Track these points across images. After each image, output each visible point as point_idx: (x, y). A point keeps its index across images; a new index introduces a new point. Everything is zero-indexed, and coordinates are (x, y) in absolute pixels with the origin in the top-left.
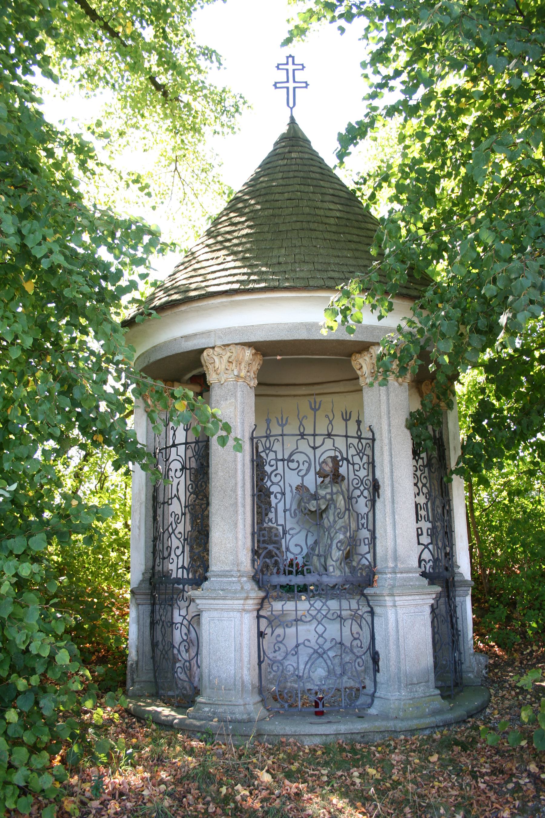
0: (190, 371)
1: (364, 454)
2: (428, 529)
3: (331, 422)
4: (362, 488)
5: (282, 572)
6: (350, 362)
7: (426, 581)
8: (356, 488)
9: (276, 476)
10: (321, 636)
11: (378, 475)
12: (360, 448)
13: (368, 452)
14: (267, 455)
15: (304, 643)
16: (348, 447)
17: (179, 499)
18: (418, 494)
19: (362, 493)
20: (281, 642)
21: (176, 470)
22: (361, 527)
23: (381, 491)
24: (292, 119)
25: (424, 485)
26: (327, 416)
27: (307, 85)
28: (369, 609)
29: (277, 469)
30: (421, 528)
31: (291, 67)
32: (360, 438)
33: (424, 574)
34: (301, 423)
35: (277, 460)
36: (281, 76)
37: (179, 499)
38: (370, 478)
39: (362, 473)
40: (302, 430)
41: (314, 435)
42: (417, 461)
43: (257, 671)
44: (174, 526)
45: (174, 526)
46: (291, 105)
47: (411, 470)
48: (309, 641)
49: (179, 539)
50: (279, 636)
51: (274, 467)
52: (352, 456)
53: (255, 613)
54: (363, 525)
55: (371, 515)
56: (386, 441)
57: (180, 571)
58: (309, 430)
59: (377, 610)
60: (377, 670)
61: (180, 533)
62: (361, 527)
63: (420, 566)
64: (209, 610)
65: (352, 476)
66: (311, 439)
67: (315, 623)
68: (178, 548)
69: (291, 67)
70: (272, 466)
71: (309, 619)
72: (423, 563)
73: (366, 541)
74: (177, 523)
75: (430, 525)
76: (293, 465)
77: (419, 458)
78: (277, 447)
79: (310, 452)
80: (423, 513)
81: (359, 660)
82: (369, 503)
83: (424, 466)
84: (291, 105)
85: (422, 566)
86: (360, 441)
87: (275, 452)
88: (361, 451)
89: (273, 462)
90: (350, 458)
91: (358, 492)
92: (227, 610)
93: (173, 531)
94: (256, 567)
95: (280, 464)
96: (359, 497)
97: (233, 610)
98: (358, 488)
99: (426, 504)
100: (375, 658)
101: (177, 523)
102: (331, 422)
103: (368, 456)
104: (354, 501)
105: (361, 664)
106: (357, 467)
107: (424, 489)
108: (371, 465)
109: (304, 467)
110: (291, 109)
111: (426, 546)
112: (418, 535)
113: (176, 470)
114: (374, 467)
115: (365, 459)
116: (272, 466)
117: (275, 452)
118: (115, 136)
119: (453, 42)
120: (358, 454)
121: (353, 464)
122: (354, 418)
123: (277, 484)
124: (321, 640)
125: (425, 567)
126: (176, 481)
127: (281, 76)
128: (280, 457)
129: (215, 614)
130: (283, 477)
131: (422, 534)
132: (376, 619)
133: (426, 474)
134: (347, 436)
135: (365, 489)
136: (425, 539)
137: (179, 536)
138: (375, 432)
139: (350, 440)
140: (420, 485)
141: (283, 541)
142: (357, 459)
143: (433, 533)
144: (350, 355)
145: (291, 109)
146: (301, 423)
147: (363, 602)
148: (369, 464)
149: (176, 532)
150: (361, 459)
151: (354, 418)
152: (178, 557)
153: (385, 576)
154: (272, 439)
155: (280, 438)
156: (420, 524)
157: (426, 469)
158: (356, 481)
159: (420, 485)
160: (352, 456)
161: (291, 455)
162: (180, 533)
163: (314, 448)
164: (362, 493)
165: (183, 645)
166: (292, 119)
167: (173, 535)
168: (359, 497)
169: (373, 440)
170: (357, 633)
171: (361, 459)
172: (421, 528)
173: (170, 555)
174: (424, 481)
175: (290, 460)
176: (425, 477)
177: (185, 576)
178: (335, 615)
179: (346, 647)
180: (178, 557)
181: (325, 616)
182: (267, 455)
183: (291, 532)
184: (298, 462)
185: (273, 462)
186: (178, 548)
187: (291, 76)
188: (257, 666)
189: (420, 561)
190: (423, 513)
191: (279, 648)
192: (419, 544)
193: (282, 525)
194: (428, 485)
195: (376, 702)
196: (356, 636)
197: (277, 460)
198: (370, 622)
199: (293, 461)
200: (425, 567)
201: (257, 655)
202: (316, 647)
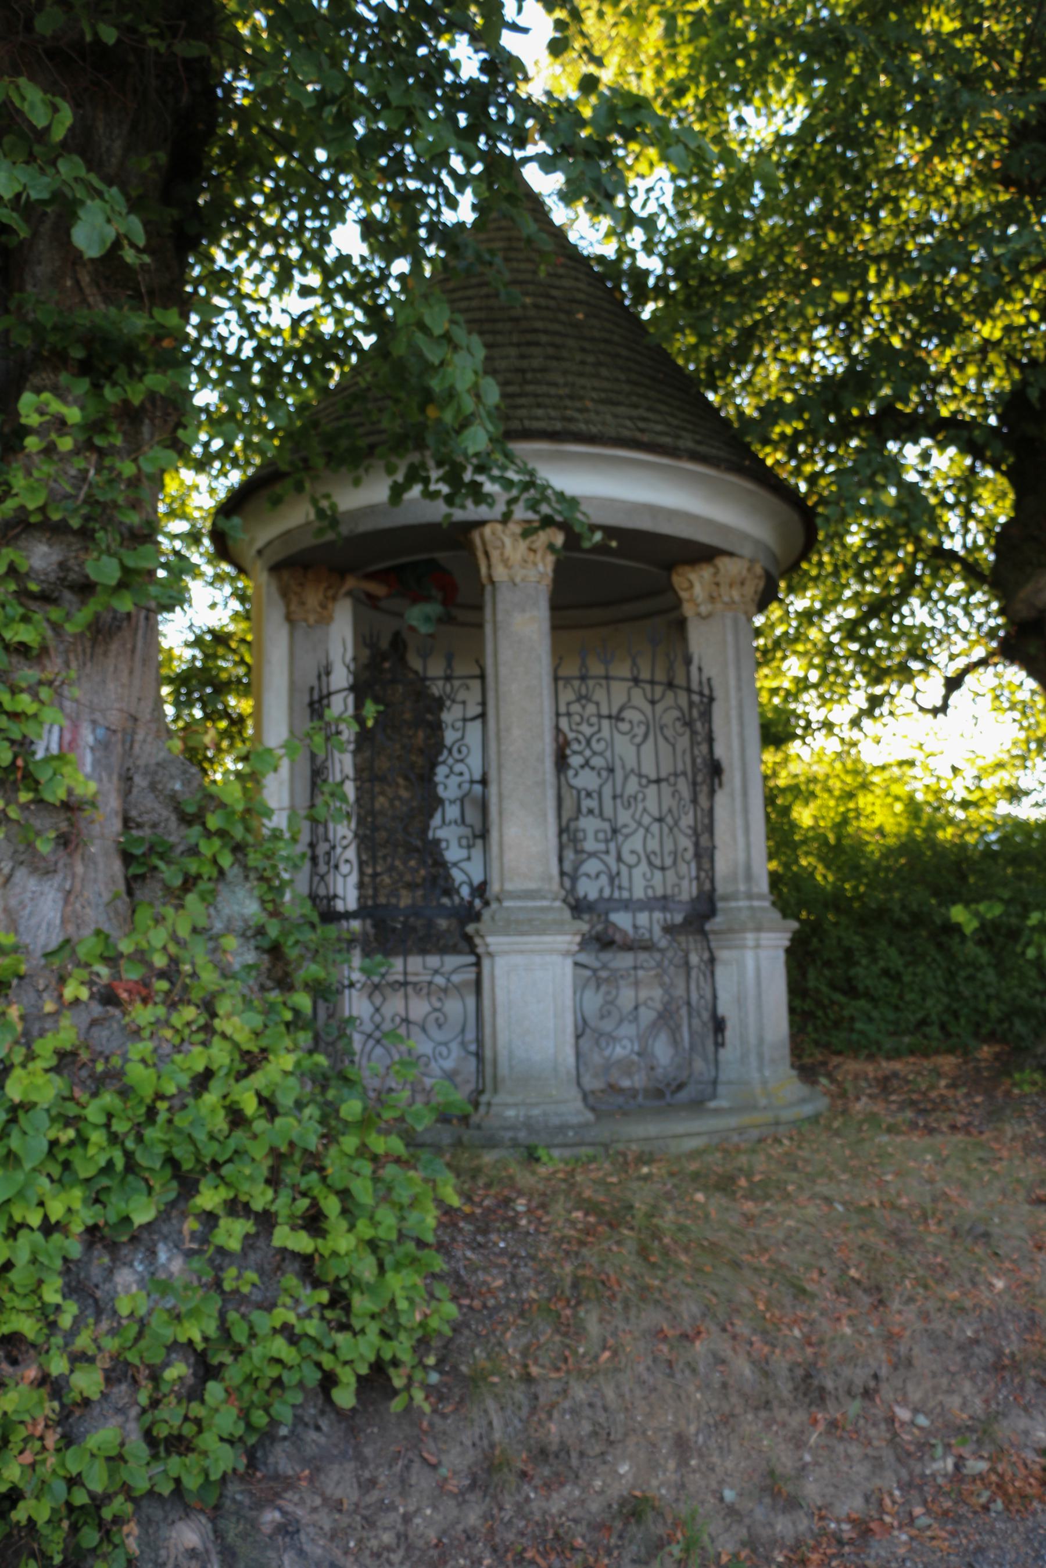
23: (725, 778)
35: (600, 716)
56: (734, 703)
58: (645, 675)
59: (722, 955)
60: (719, 1044)
64: (506, 953)
76: (624, 727)
78: (599, 695)
79: (647, 707)
92: (541, 952)
95: (605, 723)
97: (551, 952)
100: (719, 1025)
109: (641, 731)
119: (270, 260)
123: (601, 754)
128: (605, 711)
129: (518, 960)
130: (611, 744)
161: (622, 709)
163: (653, 702)
175: (619, 718)
195: (721, 1089)
197: (600, 716)
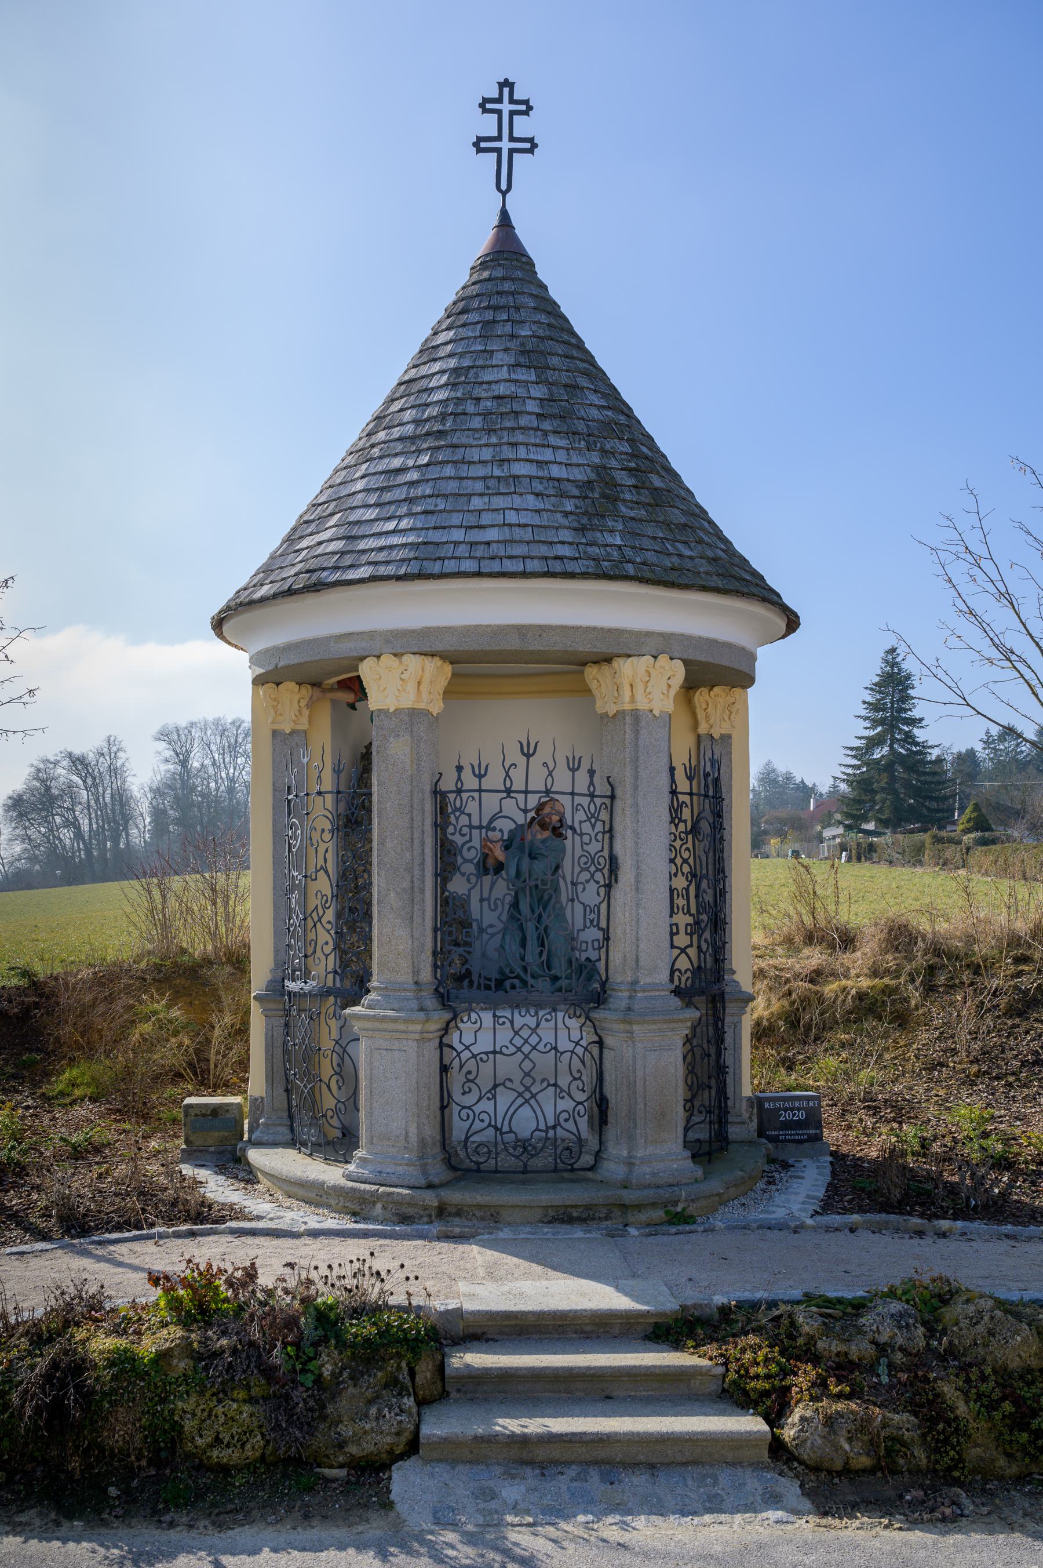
0: (341, 674)
1: (597, 819)
2: (687, 925)
3: (550, 774)
4: (593, 869)
5: (476, 984)
6: (582, 672)
7: (676, 1002)
8: (583, 870)
9: (469, 849)
10: (527, 1074)
11: (618, 849)
12: (592, 810)
13: (604, 815)
14: (457, 819)
15: (503, 1084)
16: (575, 809)
17: (326, 872)
18: (676, 875)
19: (592, 876)
20: (472, 1081)
21: (323, 831)
22: (588, 924)
24: (505, 222)
25: (685, 861)
26: (545, 764)
27: (535, 146)
28: (596, 1039)
29: (470, 840)
30: (676, 925)
31: (506, 107)
32: (592, 796)
33: (677, 992)
34: (507, 775)
35: (471, 827)
36: (488, 125)
37: (326, 872)
38: (606, 853)
39: (594, 848)
40: (508, 786)
41: (526, 792)
42: (676, 826)
43: (439, 1118)
44: (321, 913)
45: (321, 913)
46: (504, 187)
47: (665, 841)
48: (510, 1080)
49: (328, 931)
50: (469, 1072)
51: (467, 838)
52: (581, 822)
53: (437, 1041)
54: (592, 922)
55: (604, 906)
57: (331, 976)
58: (519, 785)
61: (329, 922)
62: (588, 924)
63: (672, 981)
65: (578, 852)
66: (521, 797)
67: (520, 1056)
68: (327, 943)
69: (506, 107)
70: (464, 835)
71: (513, 1049)
72: (677, 973)
73: (596, 944)
74: (324, 908)
75: (690, 920)
77: (680, 820)
80: (681, 902)
81: (580, 1107)
82: (602, 891)
83: (686, 833)
84: (504, 187)
85: (676, 979)
86: (592, 800)
87: (469, 815)
88: (593, 815)
89: (465, 830)
90: (577, 826)
91: (585, 876)
93: (320, 920)
94: (438, 976)
96: (587, 881)
98: (587, 869)
99: (687, 890)
101: (324, 908)
102: (550, 774)
103: (604, 822)
104: (580, 887)
105: (582, 1113)
106: (586, 839)
107: (685, 866)
108: (607, 836)
110: (504, 194)
111: (683, 951)
112: (672, 934)
113: (323, 831)
114: (611, 838)
115: (599, 826)
116: (464, 835)
117: (469, 815)
118: (355, 1261)
120: (589, 820)
121: (581, 835)
122: (585, 766)
124: (528, 1081)
125: (680, 980)
126: (322, 847)
127: (488, 125)
128: (475, 822)
131: (677, 933)
132: (606, 1052)
133: (690, 845)
134: (573, 794)
135: (597, 870)
136: (682, 940)
137: (329, 926)
138: (616, 785)
139: (578, 799)
140: (679, 861)
141: (478, 943)
142: (586, 827)
143: (695, 929)
144: (584, 664)
145: (504, 194)
146: (507, 775)
147: (589, 1028)
148: (604, 833)
149: (324, 920)
150: (593, 827)
151: (585, 766)
152: (327, 956)
153: (620, 994)
154: (465, 795)
155: (476, 795)
156: (676, 919)
157: (690, 837)
158: (584, 860)
159: (679, 861)
160: (581, 822)
161: (491, 821)
162: (329, 922)
164: (592, 876)
165: (335, 1078)
166: (505, 222)
167: (318, 925)
168: (587, 881)
169: (613, 797)
170: (579, 1071)
171: (593, 827)
172: (676, 925)
173: (314, 952)
174: (686, 855)
176: (687, 849)
177: (338, 985)
178: (549, 1047)
179: (562, 1091)
180: (327, 956)
181: (534, 1048)
182: (457, 819)
183: (489, 931)
184: (501, 830)
185: (465, 830)
186: (327, 943)
187: (505, 129)
188: (438, 1113)
189: (672, 972)
190: (681, 902)
191: (470, 1090)
192: (672, 946)
193: (477, 920)
194: (691, 861)
196: (577, 1075)
198: (597, 1057)
199: (494, 829)
200: (680, 980)
201: (438, 1098)
202: (521, 1089)
